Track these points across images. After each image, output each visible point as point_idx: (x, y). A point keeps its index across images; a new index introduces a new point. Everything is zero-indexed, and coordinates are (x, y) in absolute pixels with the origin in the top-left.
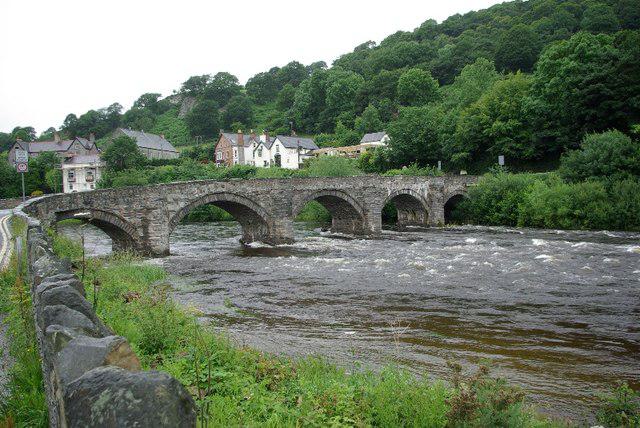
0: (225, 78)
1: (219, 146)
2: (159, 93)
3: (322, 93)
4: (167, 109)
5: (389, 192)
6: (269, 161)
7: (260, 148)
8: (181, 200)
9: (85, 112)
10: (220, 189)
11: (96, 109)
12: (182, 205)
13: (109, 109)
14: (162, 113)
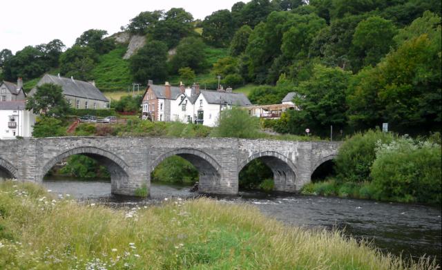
0: (177, 15)
1: (147, 98)
2: (102, 29)
3: (278, 39)
4: (113, 47)
5: (251, 154)
6: (192, 116)
7: (184, 102)
8: (54, 150)
9: (21, 49)
10: (87, 144)
11: (34, 44)
12: (55, 154)
13: (48, 46)
14: (106, 52)
